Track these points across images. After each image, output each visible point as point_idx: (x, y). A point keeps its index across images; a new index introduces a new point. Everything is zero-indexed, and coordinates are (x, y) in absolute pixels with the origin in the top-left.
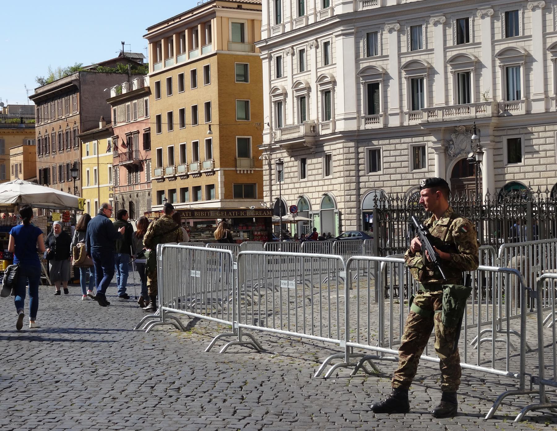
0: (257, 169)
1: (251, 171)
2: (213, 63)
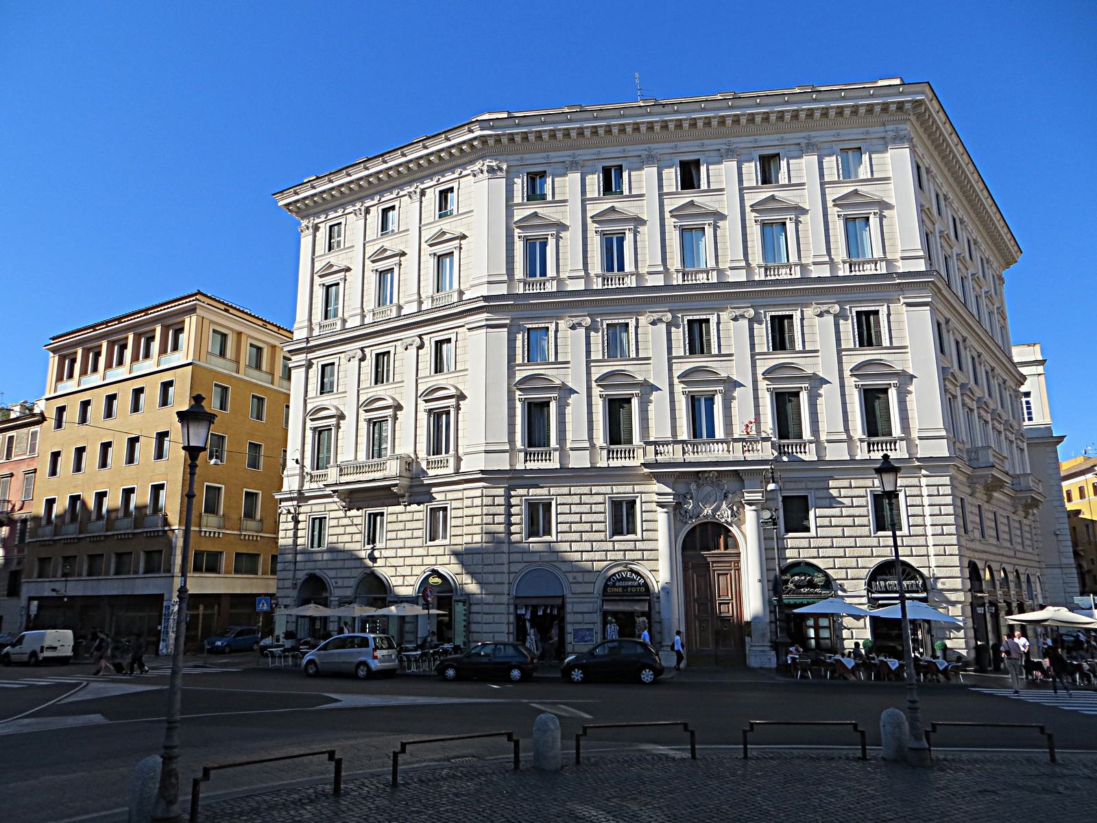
0: (227, 532)
1: (219, 533)
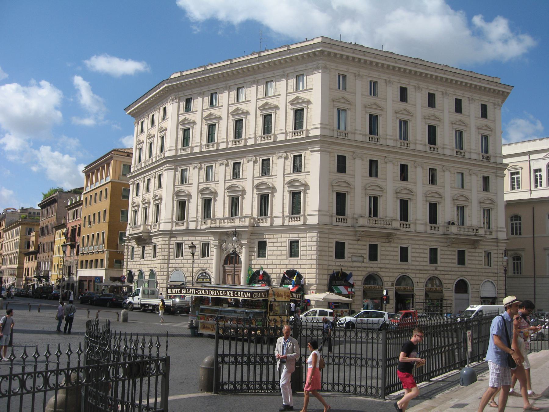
2: (109, 186)
